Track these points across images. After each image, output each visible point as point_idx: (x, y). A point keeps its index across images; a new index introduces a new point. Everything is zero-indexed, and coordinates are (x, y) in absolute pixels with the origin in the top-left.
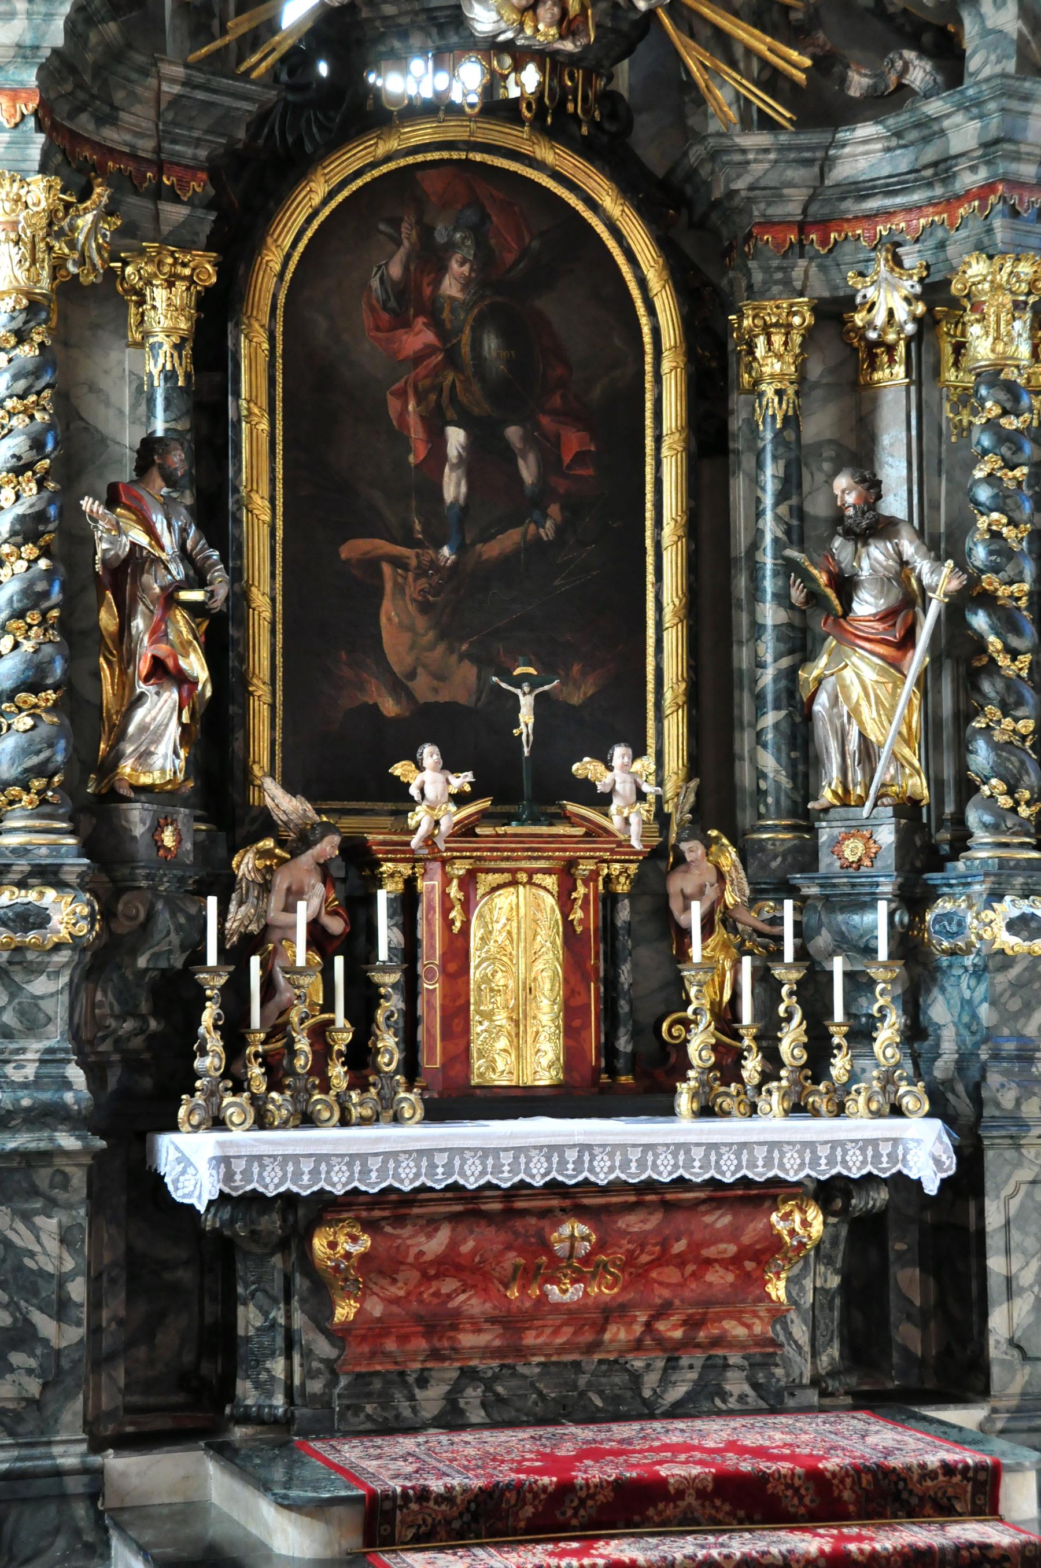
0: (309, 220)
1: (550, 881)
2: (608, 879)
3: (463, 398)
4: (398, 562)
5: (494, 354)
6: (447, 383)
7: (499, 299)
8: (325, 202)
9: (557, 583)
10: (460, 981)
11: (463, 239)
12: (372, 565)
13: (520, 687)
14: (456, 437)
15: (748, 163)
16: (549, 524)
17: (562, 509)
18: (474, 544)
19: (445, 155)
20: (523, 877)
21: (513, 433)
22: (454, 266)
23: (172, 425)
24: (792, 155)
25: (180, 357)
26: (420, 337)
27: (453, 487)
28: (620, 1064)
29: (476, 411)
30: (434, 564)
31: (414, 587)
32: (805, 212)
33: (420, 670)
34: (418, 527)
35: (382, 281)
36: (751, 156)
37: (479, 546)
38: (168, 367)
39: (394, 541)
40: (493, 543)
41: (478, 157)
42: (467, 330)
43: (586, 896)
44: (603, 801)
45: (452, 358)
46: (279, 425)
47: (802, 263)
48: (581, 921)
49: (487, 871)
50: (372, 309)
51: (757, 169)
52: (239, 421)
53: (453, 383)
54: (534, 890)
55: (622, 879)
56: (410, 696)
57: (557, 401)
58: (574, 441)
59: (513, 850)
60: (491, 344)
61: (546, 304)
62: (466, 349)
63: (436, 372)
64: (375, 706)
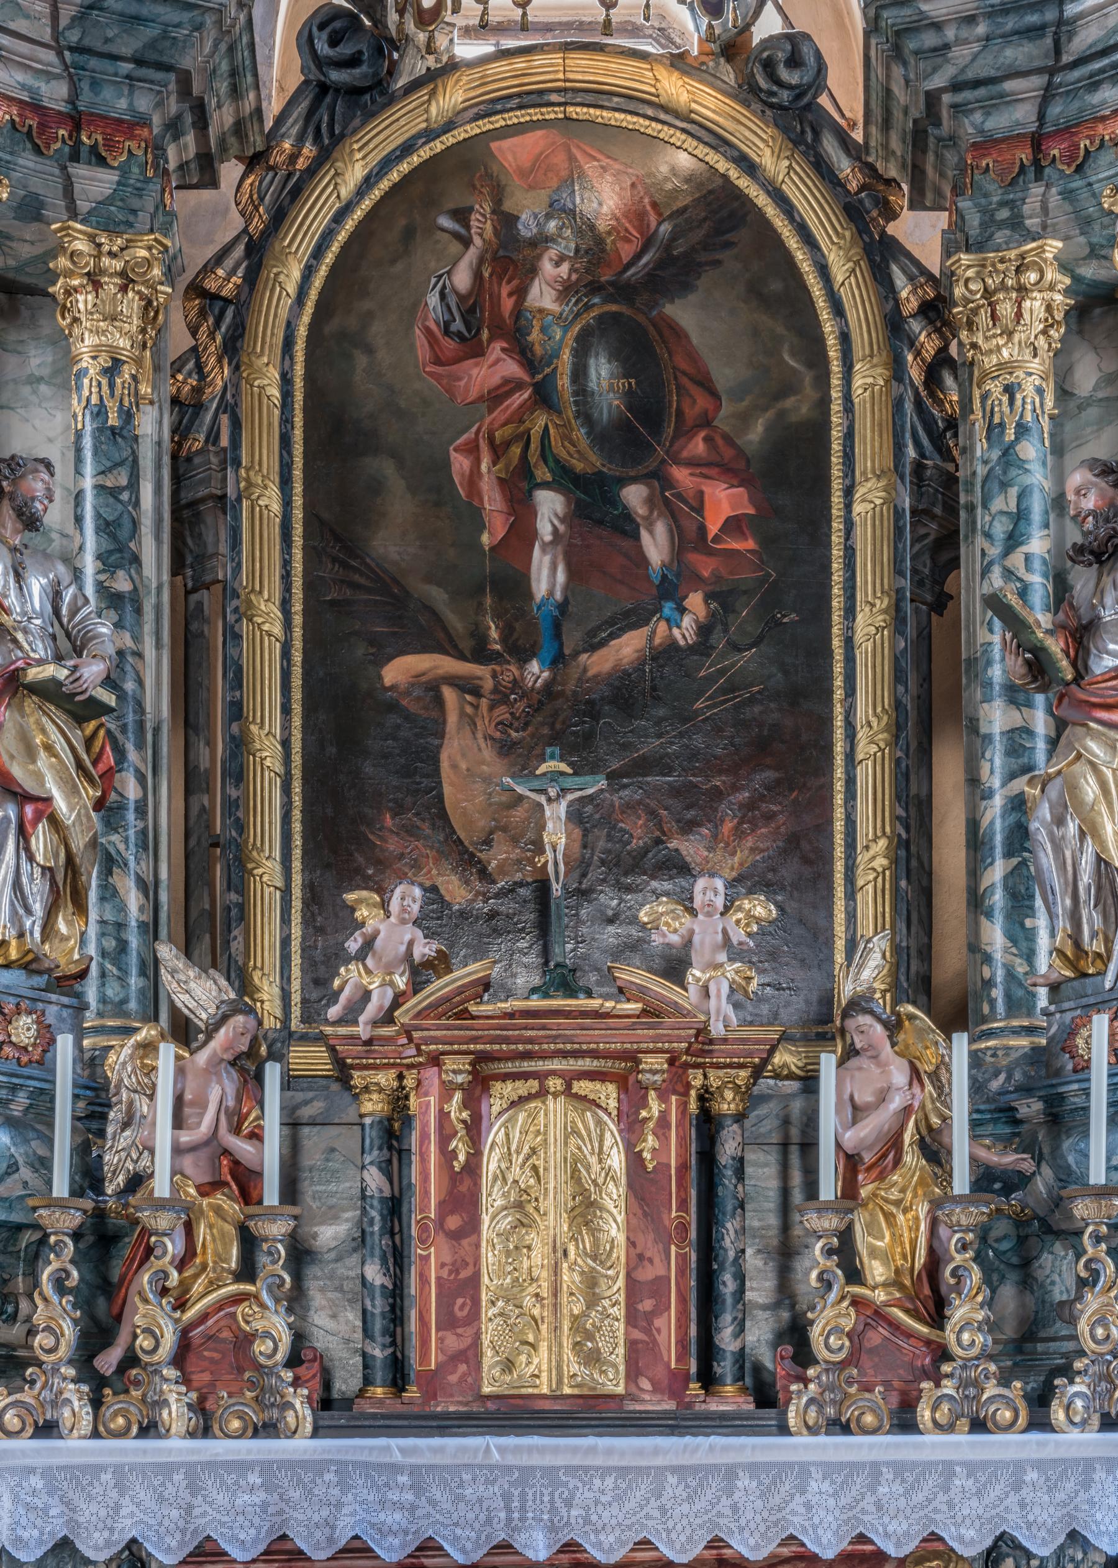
2: (704, 1097)
3: (559, 448)
4: (468, 687)
5: (605, 384)
6: (536, 431)
7: (614, 308)
8: (362, 191)
9: (699, 705)
10: (465, 1242)
12: (432, 688)
14: (549, 507)
15: (947, 47)
16: (687, 621)
17: (708, 597)
18: (576, 654)
20: (555, 1084)
21: (634, 496)
22: (547, 266)
23: (101, 480)
25: (112, 386)
26: (497, 366)
27: (546, 577)
29: (579, 466)
32: (1041, 117)
34: (494, 634)
35: (443, 296)
36: (950, 33)
37: (584, 656)
38: (94, 400)
39: (462, 657)
40: (603, 651)
42: (566, 356)
47: (1037, 190)
49: (505, 1077)
50: (428, 331)
51: (961, 54)
52: (239, 499)
53: (546, 428)
55: (729, 1095)
57: (698, 446)
58: (724, 501)
60: (602, 372)
61: (683, 313)
62: (564, 382)
63: (519, 417)
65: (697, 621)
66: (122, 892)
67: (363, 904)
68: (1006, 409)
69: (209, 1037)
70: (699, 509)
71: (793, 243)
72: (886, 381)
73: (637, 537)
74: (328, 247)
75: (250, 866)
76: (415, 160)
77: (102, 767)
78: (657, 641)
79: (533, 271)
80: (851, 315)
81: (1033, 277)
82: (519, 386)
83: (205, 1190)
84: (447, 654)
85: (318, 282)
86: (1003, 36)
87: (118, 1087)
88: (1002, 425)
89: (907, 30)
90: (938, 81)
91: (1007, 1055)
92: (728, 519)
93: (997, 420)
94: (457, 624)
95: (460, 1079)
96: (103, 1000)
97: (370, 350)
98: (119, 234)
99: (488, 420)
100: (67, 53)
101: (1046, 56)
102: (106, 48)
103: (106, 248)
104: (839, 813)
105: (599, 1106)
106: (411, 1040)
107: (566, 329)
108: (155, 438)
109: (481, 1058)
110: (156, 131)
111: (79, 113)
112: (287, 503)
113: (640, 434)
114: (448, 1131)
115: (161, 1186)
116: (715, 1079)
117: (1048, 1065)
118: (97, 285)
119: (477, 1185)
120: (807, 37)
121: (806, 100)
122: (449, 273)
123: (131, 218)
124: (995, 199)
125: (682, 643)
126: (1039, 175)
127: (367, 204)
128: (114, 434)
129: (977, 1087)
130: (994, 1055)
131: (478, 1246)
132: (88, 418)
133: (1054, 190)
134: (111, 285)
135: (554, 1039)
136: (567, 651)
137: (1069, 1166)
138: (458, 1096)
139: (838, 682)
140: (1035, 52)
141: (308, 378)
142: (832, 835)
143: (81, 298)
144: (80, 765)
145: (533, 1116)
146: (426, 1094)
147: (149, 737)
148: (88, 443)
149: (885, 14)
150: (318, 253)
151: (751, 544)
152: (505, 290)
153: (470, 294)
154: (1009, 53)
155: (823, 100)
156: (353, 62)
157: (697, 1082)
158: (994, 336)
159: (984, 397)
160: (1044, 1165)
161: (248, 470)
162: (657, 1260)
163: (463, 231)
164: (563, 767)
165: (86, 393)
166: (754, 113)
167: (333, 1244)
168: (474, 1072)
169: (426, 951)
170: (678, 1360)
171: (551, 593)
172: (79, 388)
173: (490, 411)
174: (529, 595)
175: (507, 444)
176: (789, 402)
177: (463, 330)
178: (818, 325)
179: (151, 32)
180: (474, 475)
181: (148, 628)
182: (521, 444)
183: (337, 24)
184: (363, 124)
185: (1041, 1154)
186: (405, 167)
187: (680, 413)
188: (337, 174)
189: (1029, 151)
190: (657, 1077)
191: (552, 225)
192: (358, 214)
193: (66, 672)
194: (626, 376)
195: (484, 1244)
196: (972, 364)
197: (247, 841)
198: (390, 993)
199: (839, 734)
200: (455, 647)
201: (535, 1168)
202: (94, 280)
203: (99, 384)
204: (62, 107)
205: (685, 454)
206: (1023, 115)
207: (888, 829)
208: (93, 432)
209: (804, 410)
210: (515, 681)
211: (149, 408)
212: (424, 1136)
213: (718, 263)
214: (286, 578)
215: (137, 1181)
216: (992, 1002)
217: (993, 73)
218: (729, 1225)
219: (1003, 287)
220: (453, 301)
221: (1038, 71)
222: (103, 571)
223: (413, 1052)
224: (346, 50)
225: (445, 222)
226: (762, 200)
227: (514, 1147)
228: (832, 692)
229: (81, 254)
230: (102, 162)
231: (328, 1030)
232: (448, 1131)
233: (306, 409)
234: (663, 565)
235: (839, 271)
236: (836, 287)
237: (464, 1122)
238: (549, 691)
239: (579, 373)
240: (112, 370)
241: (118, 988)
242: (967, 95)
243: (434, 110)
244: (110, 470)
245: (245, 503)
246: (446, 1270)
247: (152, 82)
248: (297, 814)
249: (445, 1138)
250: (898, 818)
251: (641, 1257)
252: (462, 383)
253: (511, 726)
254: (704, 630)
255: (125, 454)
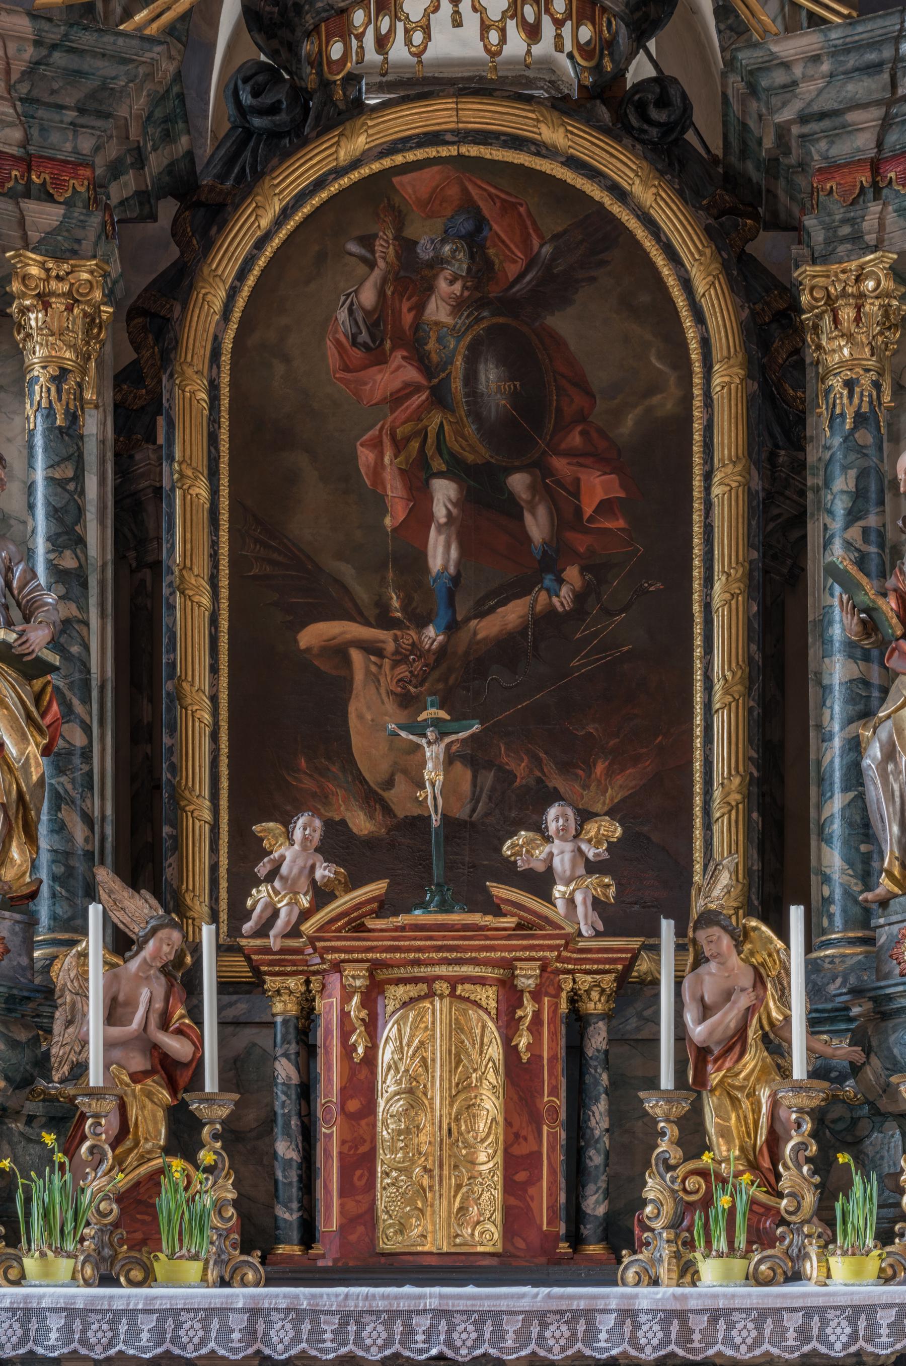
0: (260, 244)
1: (488, 996)
2: (574, 999)
4: (371, 649)
5: (493, 386)
7: (501, 320)
9: (575, 663)
10: (363, 1122)
11: (453, 252)
12: (339, 652)
13: (424, 735)
14: (444, 494)
16: (564, 591)
17: (583, 570)
18: (468, 620)
19: (431, 152)
20: (442, 987)
22: (442, 285)
23: (50, 473)
24: (852, 61)
25: (59, 391)
26: (398, 372)
27: (441, 553)
28: (588, 1230)
29: (470, 458)
30: (415, 647)
31: (390, 676)
32: (880, 144)
33: (399, 778)
34: (395, 603)
35: (351, 311)
36: (798, 71)
37: (474, 623)
39: (368, 624)
41: (473, 151)
42: (459, 362)
43: (537, 1015)
44: (540, 883)
45: (440, 397)
46: (224, 491)
47: (875, 208)
48: (529, 1047)
49: (398, 982)
50: (338, 343)
51: (808, 89)
52: (173, 489)
53: (441, 425)
54: (458, 1004)
55: (595, 995)
56: (387, 810)
57: (575, 439)
58: (597, 487)
59: (419, 949)
60: (490, 376)
61: (561, 323)
62: (457, 386)
63: (417, 416)
64: (343, 822)
65: (573, 591)
66: (69, 825)
67: (267, 829)
68: (845, 400)
69: (141, 949)
70: (576, 494)
71: (660, 261)
72: (742, 380)
73: (521, 518)
74: (250, 270)
75: (183, 803)
76: (324, 195)
77: (49, 719)
78: (538, 608)
79: (429, 289)
80: (711, 323)
81: (871, 284)
82: (418, 389)
83: (136, 1078)
84: (355, 621)
85: (241, 303)
86: (845, 73)
87: (62, 990)
88: (842, 415)
89: (759, 69)
90: (786, 115)
91: (843, 962)
92: (601, 502)
93: (838, 411)
94: (363, 595)
95: (358, 983)
96: (54, 917)
97: (286, 359)
98: (65, 260)
99: (390, 419)
100: (18, 103)
101: (884, 89)
102: (51, 100)
103: (54, 274)
104: (698, 754)
105: (480, 1006)
106: (315, 949)
107: (459, 339)
108: (100, 437)
109: (375, 966)
110: (98, 171)
111: (30, 155)
112: (214, 492)
113: (524, 431)
114: (347, 1028)
115: (95, 1077)
116: (585, 981)
117: (878, 970)
118: (46, 306)
119: (374, 1073)
120: (675, 81)
121: (673, 136)
122: (356, 291)
123: (76, 247)
124: (838, 217)
125: (560, 609)
126: (877, 192)
127: (283, 234)
128: (61, 433)
129: (814, 990)
130: (831, 962)
131: (374, 1126)
132: (39, 420)
133: (890, 208)
134: (58, 304)
135: (439, 949)
136: (459, 618)
137: (895, 1057)
138: (356, 1000)
139: (698, 641)
140: (874, 86)
141: (234, 384)
142: (691, 774)
143: (32, 316)
144: (29, 717)
145: (421, 1016)
146: (330, 997)
147: (95, 694)
148: (39, 441)
149: (740, 55)
150: (242, 275)
151: (621, 523)
152: (405, 306)
153: (375, 309)
154: (850, 87)
155: (690, 136)
156: (273, 109)
157: (568, 986)
158: (835, 338)
159: (828, 391)
160: (872, 1055)
161: (180, 463)
162: (531, 1138)
163: (368, 255)
164: (443, 714)
165: (37, 398)
166: (625, 147)
167: (254, 1125)
168: (371, 976)
169: (327, 873)
170: (548, 1224)
171: (445, 568)
172: (32, 394)
173: (392, 412)
174: (426, 569)
175: (408, 439)
176: (656, 399)
177: (369, 341)
178: (682, 332)
179: (91, 84)
180: (379, 464)
181: (93, 601)
182: (419, 440)
183: (260, 78)
184: (281, 163)
185: (870, 1047)
186: (316, 201)
187: (559, 410)
188: (257, 207)
189: (869, 174)
190: (530, 981)
191: (447, 248)
192: (276, 242)
193: (15, 636)
194: (512, 379)
195: (379, 1124)
196: (818, 362)
197: (179, 782)
198: (296, 912)
199: (698, 686)
200: (361, 613)
201: (424, 1060)
202: (44, 300)
203: (49, 390)
204: (14, 151)
205: (563, 446)
206: (863, 142)
207: (741, 769)
208: (44, 431)
209: (669, 406)
210: (413, 644)
211: (94, 412)
212: (328, 1032)
213: (593, 279)
214: (214, 557)
215: (80, 1069)
216: (831, 917)
217: (836, 106)
218: (594, 1108)
219: (844, 294)
220: (359, 316)
221: (877, 103)
222: (53, 551)
223: (318, 960)
224: (267, 99)
225: (353, 247)
226: (633, 224)
227: (405, 1042)
228: (692, 651)
229: (31, 276)
230: (50, 199)
231: (243, 942)
232: (347, 1028)
233: (231, 411)
234: (544, 542)
235: (700, 285)
236: (698, 298)
237: (363, 1020)
238: (443, 650)
239: (471, 378)
240: (60, 378)
241: (66, 907)
242: (813, 127)
243: (342, 153)
244: (58, 464)
245: (178, 493)
246: (347, 1146)
247: (93, 128)
248: (224, 761)
249: (345, 1035)
250: (750, 759)
251: (517, 1135)
252: (368, 387)
253: (410, 682)
254: (580, 598)
255: (71, 451)
